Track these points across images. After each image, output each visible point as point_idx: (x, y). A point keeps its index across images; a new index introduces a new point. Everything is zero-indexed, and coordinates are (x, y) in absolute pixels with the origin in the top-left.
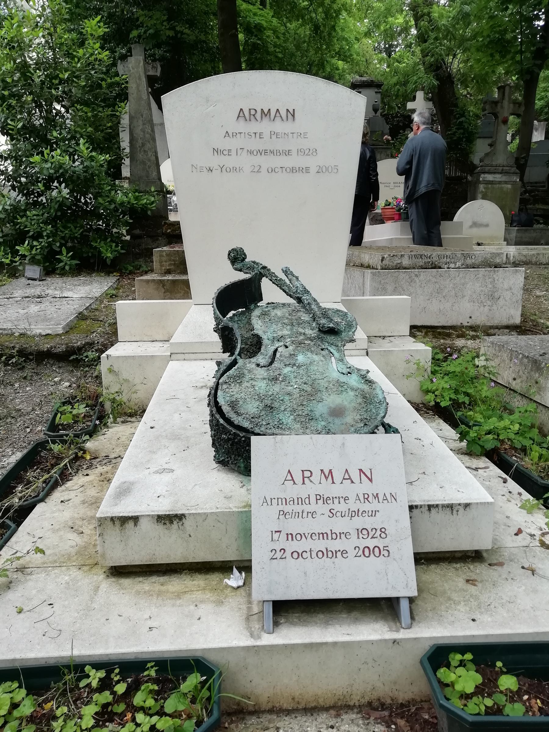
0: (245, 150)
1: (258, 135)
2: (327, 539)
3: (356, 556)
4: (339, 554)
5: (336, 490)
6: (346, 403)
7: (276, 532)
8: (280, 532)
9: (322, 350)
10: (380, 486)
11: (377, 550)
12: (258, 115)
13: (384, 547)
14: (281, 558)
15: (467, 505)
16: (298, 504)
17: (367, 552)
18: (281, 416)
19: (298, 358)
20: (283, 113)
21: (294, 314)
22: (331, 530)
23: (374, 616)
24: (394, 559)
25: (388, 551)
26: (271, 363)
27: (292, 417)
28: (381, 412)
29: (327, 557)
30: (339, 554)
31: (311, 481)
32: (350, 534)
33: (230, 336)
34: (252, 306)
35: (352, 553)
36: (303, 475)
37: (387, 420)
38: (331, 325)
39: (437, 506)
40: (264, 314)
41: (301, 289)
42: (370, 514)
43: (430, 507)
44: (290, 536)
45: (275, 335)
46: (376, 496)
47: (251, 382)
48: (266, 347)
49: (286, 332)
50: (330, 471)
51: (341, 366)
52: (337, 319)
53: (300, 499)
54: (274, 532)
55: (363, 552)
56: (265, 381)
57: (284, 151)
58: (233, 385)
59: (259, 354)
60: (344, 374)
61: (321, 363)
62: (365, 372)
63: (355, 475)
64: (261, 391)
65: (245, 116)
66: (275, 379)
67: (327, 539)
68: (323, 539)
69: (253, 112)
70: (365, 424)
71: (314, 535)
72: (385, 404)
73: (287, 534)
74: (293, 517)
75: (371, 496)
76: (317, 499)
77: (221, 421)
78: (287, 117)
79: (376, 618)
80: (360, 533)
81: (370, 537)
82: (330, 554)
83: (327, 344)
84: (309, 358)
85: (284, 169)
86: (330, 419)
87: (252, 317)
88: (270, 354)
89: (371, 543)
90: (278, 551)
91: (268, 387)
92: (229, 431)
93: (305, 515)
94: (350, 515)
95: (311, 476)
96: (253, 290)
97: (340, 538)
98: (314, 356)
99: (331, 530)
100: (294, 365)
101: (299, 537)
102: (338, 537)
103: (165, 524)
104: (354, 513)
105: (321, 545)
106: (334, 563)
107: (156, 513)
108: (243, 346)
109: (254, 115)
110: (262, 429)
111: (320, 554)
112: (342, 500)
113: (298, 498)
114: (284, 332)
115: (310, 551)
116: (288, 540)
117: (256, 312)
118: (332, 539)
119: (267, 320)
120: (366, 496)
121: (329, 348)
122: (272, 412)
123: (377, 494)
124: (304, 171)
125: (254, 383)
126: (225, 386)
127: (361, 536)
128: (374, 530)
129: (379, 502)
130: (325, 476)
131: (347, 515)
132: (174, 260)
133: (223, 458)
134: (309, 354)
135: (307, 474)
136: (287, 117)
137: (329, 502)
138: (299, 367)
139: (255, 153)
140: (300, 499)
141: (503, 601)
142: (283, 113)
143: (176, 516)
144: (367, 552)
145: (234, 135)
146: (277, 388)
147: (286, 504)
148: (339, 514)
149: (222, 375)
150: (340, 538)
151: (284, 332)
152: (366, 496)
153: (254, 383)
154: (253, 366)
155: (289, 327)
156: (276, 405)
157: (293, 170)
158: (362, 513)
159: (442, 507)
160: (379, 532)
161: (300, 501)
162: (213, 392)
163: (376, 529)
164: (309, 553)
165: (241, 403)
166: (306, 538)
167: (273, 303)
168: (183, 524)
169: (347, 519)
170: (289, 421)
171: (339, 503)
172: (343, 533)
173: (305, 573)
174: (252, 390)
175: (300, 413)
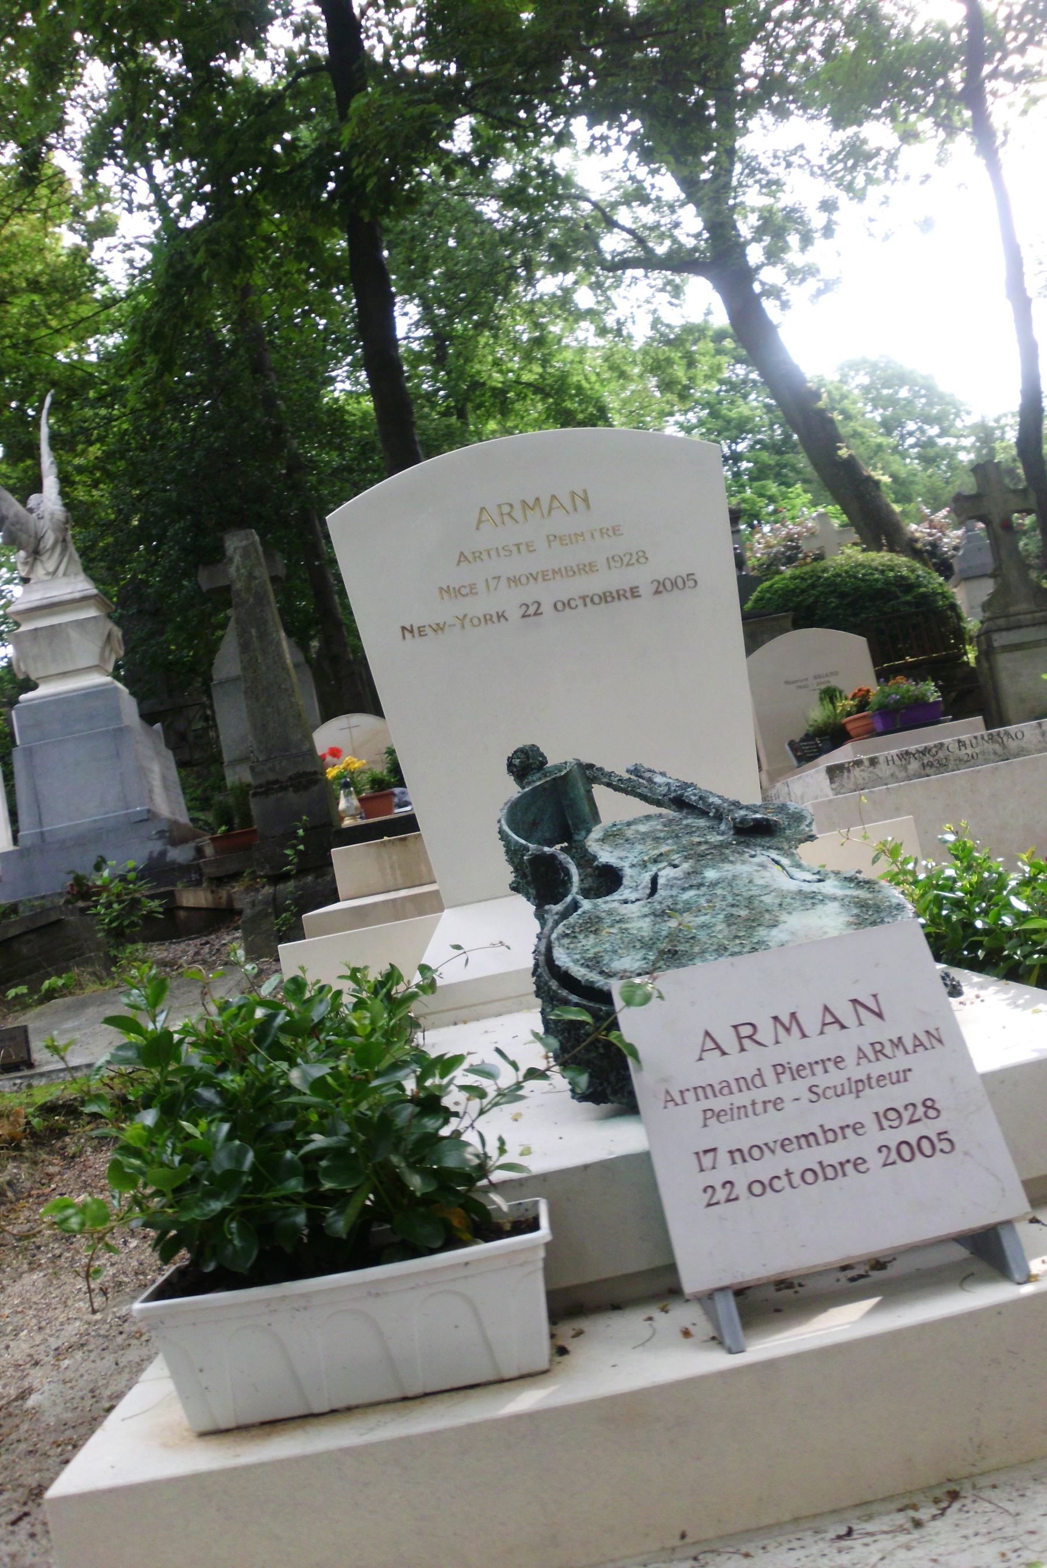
0: (503, 582)
1: (523, 548)
3: (885, 1165)
4: (849, 1168)
5: (818, 1047)
8: (714, 1150)
11: (925, 1144)
12: (518, 513)
16: (740, 1091)
29: (826, 1178)
30: (849, 1168)
32: (865, 1161)
35: (875, 1160)
42: (894, 1079)
44: (737, 1155)
46: (898, 1043)
50: (793, 1015)
75: (888, 1045)
76: (778, 1074)
80: (883, 1120)
82: (830, 1173)
85: (588, 600)
89: (911, 1134)
90: (718, 1187)
93: (759, 1108)
94: (854, 1089)
101: (756, 1153)
109: (509, 514)
111: (810, 1177)
112: (830, 1065)
116: (734, 1163)
123: (900, 1039)
127: (886, 1123)
128: (911, 1108)
129: (907, 1053)
131: (847, 1091)
137: (803, 1073)
139: (524, 580)
144: (906, 1151)
145: (477, 556)
148: (830, 1093)
157: (606, 598)
158: (878, 1081)
160: (921, 1110)
161: (744, 1083)
163: (914, 1105)
164: (785, 1179)
166: (773, 1152)
169: (849, 1098)
171: (826, 1071)
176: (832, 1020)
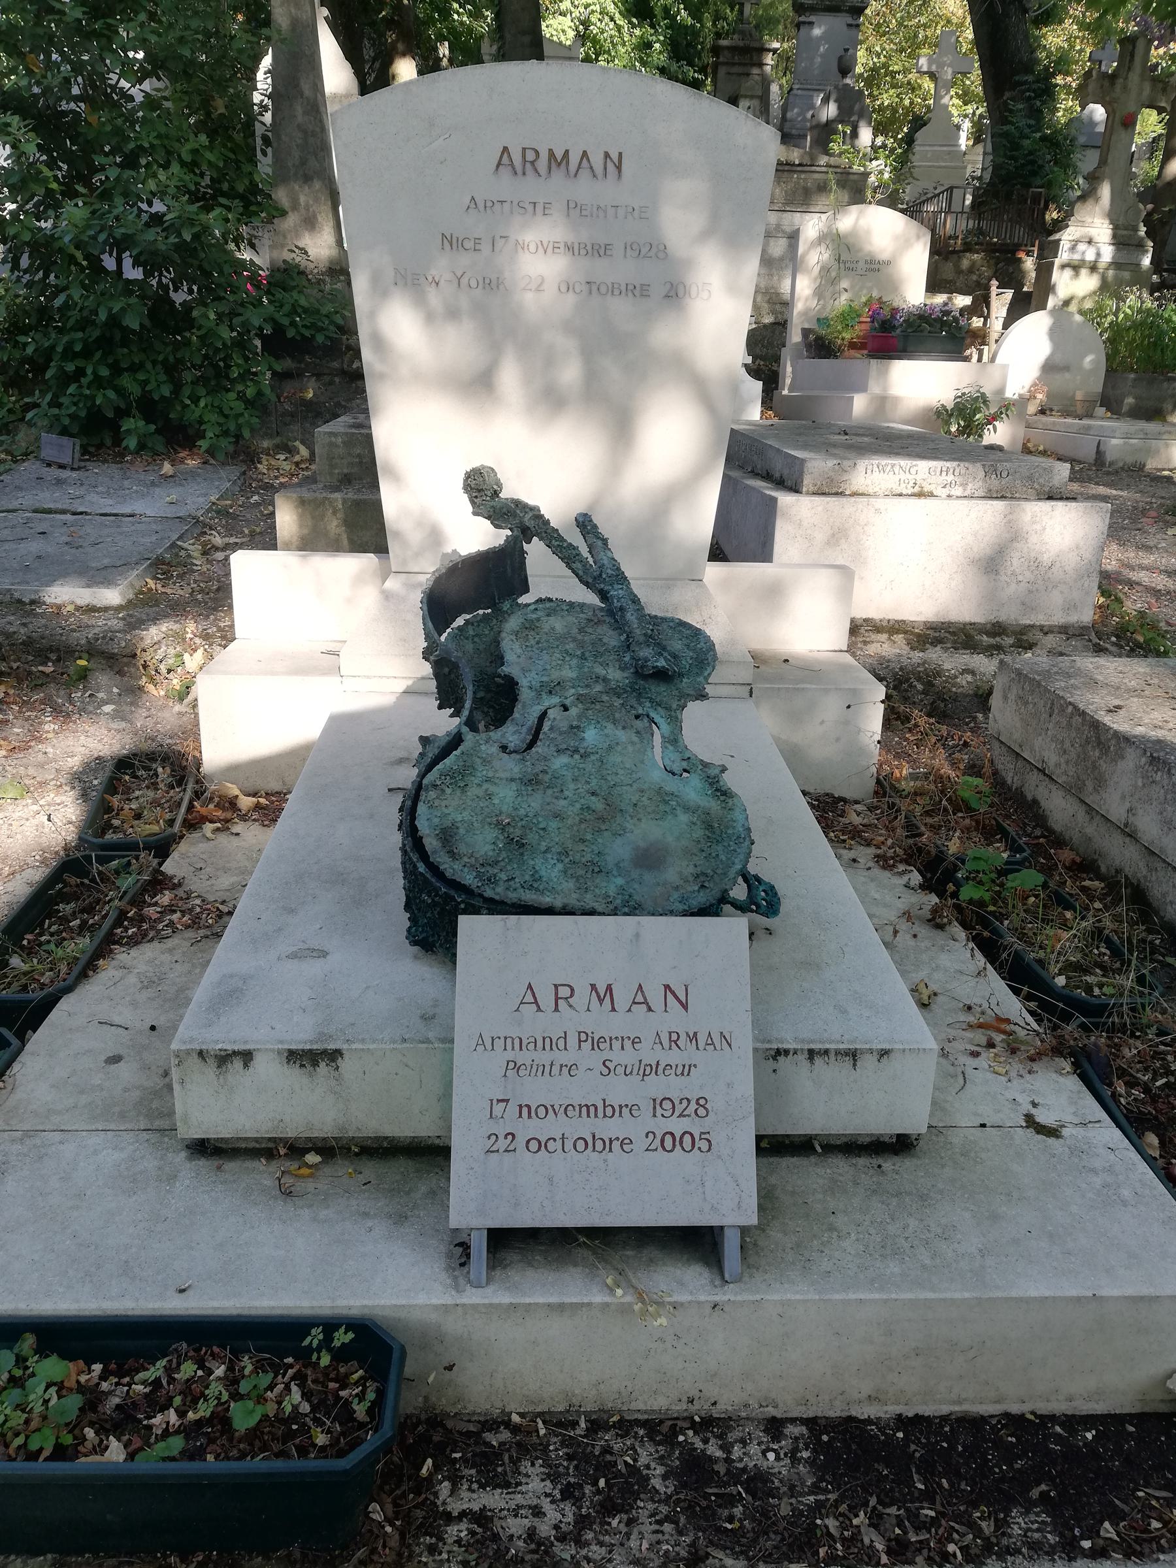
2: (596, 1116)
4: (616, 1145)
6: (670, 839)
7: (499, 1101)
9: (637, 717)
10: (702, 1019)
11: (687, 1138)
13: (702, 1133)
14: (506, 1151)
15: (884, 1053)
17: (671, 1142)
18: (538, 862)
19: (585, 735)
20: (597, 160)
21: (590, 630)
22: (604, 1101)
23: (685, 1257)
24: (719, 1157)
25: (709, 1141)
26: (531, 745)
27: (560, 866)
28: (736, 861)
30: (616, 1145)
31: (571, 1006)
33: (453, 676)
34: (506, 606)
35: (640, 1143)
36: (556, 994)
37: (752, 869)
38: (661, 663)
39: (826, 1052)
40: (530, 626)
41: (609, 571)
42: (679, 1071)
43: (812, 1054)
45: (545, 679)
47: (485, 786)
48: (524, 707)
49: (569, 673)
50: (609, 988)
51: (671, 755)
52: (677, 645)
53: (547, 1040)
54: (495, 1102)
55: (662, 1141)
56: (514, 786)
57: (596, 247)
58: (448, 791)
59: (508, 723)
60: (674, 774)
61: (630, 748)
62: (717, 771)
63: (655, 996)
64: (504, 808)
65: (512, 165)
66: (531, 782)
67: (596, 1116)
68: (588, 1116)
69: (530, 156)
70: (703, 886)
71: (570, 1108)
72: (747, 843)
73: (520, 1106)
74: (533, 1073)
75: (683, 1037)
76: (580, 1041)
77: (421, 867)
78: (605, 169)
79: (688, 1260)
80: (658, 1107)
81: (677, 1113)
83: (648, 704)
84: (607, 736)
85: (594, 288)
86: (635, 874)
87: (503, 635)
88: (530, 723)
89: (677, 1126)
90: (501, 1137)
91: (519, 799)
92: (437, 890)
94: (641, 1072)
95: (572, 996)
96: (509, 570)
97: (620, 1115)
98: (617, 732)
99: (604, 1101)
100: (576, 751)
101: (542, 1111)
102: (617, 1113)
103: (302, 1066)
104: (648, 1069)
105: (584, 1127)
106: (605, 1161)
107: (286, 1047)
108: (481, 694)
110: (499, 890)
111: (581, 1145)
112: (628, 1043)
113: (544, 1039)
114: (564, 673)
115: (563, 1138)
116: (520, 1116)
117: (513, 623)
118: (605, 1116)
119: (533, 642)
120: (674, 1037)
121: (652, 714)
122: (522, 854)
124: (637, 292)
125: (492, 789)
126: (432, 794)
127: (659, 1111)
128: (685, 1102)
130: (599, 996)
131: (635, 1072)
132: (359, 456)
133: (424, 935)
134: (610, 726)
135: (564, 992)
136: (605, 169)
137: (602, 1046)
138: (584, 756)
140: (547, 1040)
141: (928, 1235)
142: (597, 160)
143: (324, 1052)
146: (535, 803)
147: (521, 1049)
148: (620, 1070)
149: (429, 768)
150: (620, 1115)
151: (564, 673)
152: (674, 1037)
153: (492, 789)
154: (494, 749)
155: (574, 662)
156: (532, 838)
159: (836, 1054)
160: (693, 1106)
161: (549, 1043)
162: (409, 803)
165: (462, 831)
167: (550, 600)
168: (337, 1068)
170: (553, 875)
172: (627, 1106)
173: (551, 1179)
174: (487, 803)
175: (577, 857)
176: (641, 1000)
